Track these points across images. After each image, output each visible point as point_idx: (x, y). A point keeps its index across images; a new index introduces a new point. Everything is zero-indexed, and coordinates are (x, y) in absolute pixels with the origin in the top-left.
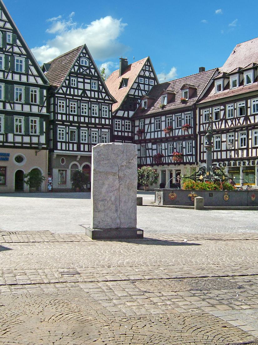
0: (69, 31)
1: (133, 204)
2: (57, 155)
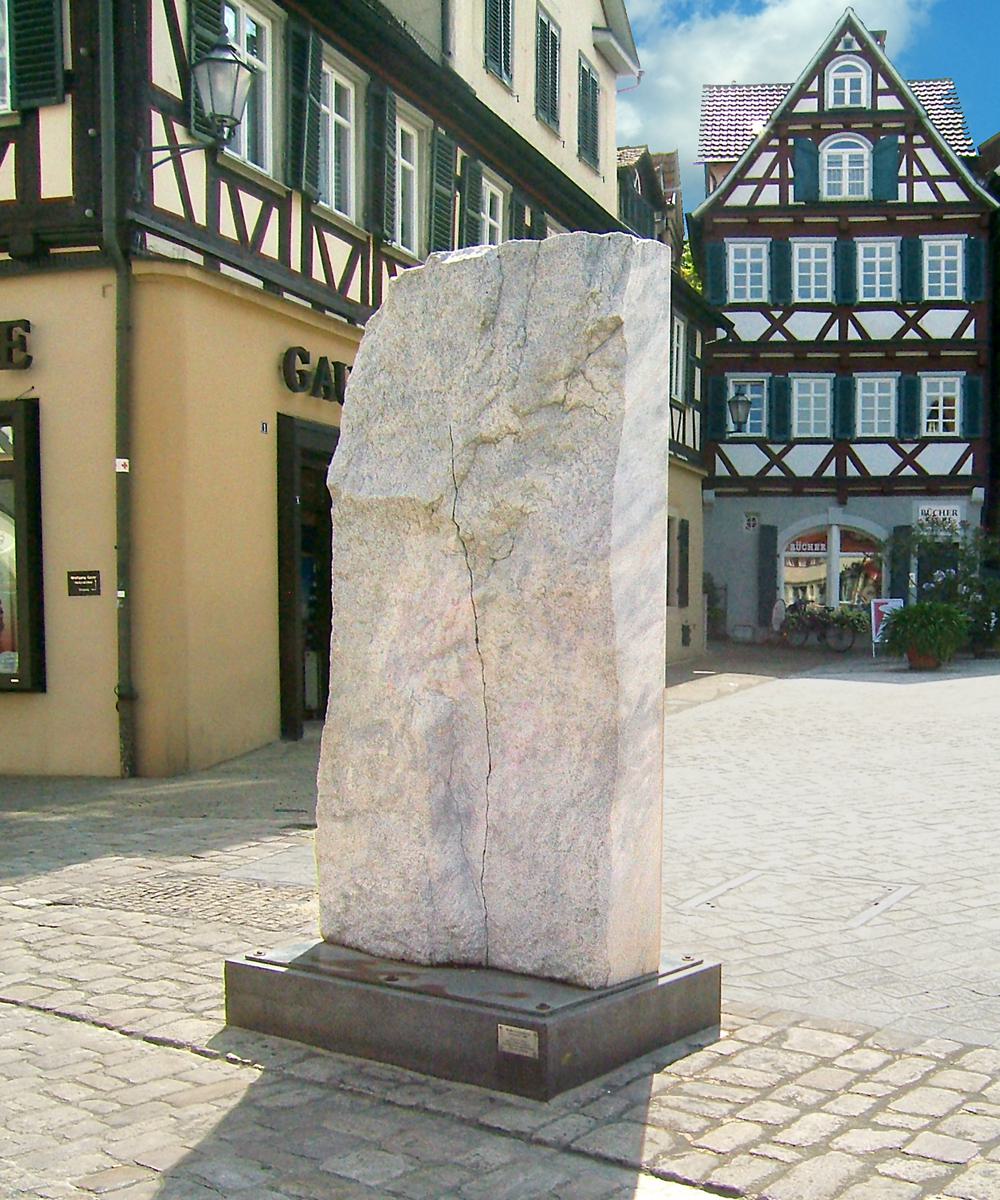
0: (682, 25)
1: (588, 773)
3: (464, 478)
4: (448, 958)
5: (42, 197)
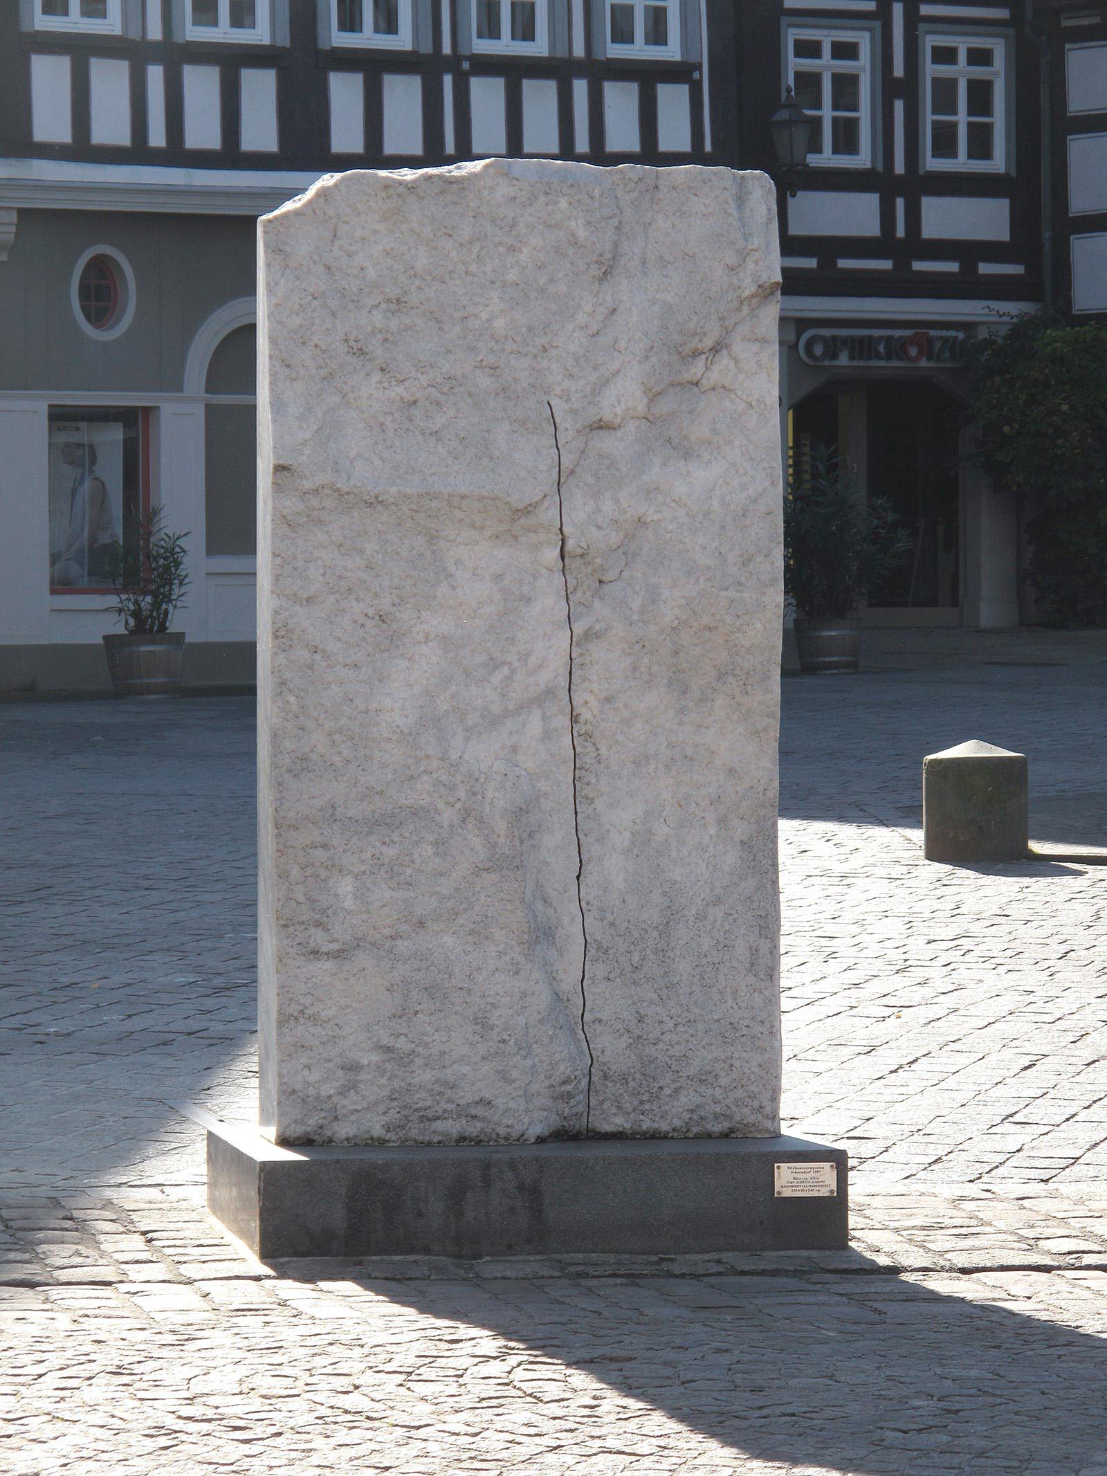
2: (22, 212)
3: (572, 473)
4: (125, 1221)
5: (1006, 202)
